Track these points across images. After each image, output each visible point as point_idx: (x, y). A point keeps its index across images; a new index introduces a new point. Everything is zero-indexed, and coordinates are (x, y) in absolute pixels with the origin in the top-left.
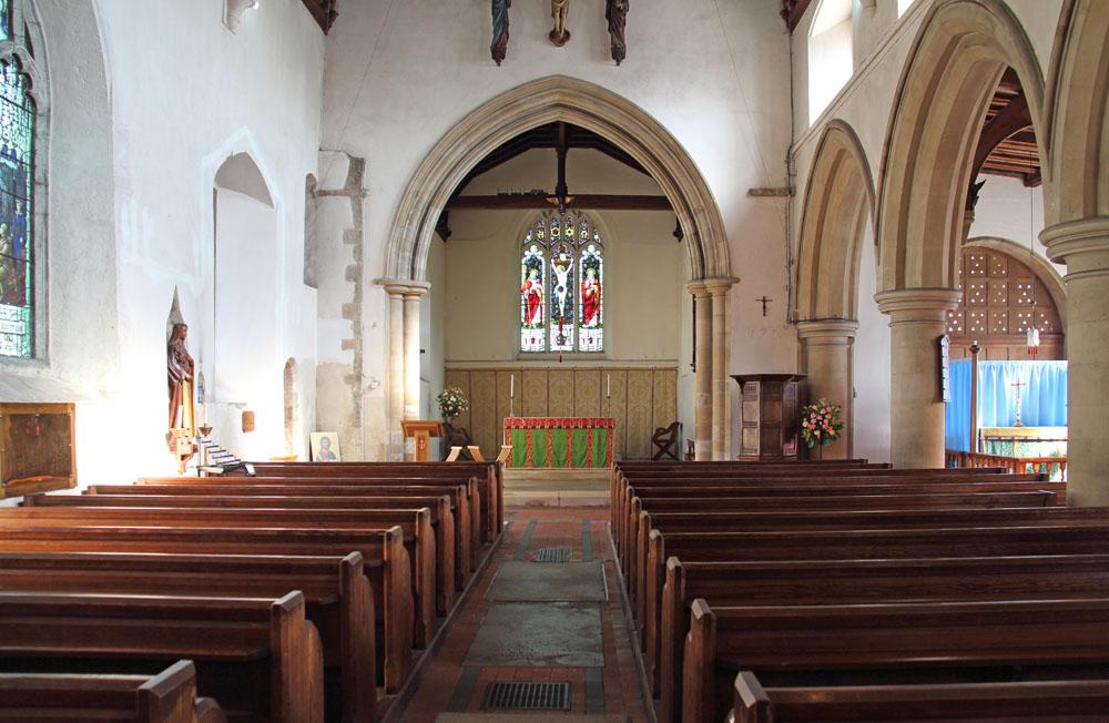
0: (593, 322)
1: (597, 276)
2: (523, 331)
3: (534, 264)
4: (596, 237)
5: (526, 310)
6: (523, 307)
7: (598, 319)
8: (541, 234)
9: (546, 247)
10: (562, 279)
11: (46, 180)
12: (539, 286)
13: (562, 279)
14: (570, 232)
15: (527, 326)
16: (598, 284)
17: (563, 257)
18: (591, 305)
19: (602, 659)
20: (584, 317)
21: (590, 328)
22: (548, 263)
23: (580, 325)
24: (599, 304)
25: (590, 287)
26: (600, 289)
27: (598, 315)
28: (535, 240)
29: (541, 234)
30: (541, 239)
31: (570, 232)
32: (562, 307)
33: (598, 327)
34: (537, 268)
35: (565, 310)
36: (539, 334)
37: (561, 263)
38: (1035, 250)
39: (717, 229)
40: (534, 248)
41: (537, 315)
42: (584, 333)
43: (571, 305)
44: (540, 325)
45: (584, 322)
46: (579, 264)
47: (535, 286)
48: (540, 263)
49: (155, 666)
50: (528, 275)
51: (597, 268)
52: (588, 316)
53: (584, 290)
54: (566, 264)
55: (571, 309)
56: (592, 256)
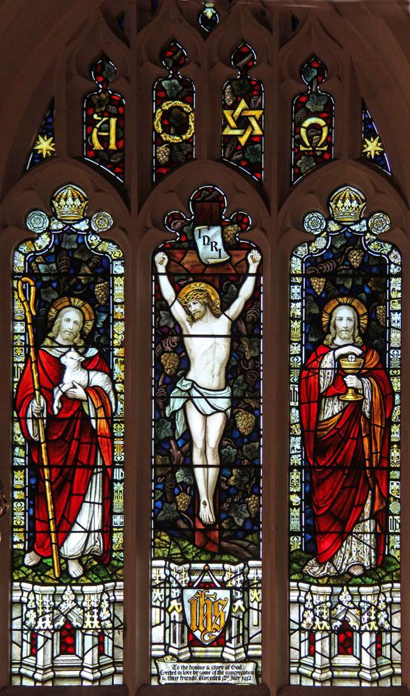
0: (356, 551)
1: (372, 336)
2: (22, 591)
3: (71, 273)
4: (372, 147)
5: (35, 494)
6: (19, 479)
7: (381, 536)
8: (106, 133)
9: (125, 184)
10: (208, 353)
11: (20, 409)
12: (99, 379)
13: (208, 353)
14: (244, 122)
15: (40, 568)
16: (379, 374)
17: (210, 244)
18: (344, 473)
19: (308, 103)
20: (310, 530)
21: (342, 579)
22: (141, 274)
23: (287, 568)
24: (384, 468)
25: (339, 386)
26: (387, 394)
27: (381, 517)
28: (74, 152)
29: (106, 133)
30: (105, 155)
31: (244, 122)
32: (205, 479)
33: (378, 572)
34: (88, 297)
35: (220, 495)
36: (93, 603)
37: (204, 273)
38: (72, 535)
39: (236, 554)
40: (69, 202)
41: (89, 516)
42: (309, 601)
43: (251, 470)
44: (99, 565)
45: (313, 551)
46: (287, 278)
47: (75, 378)
48: (102, 269)
49: (235, 564)
50: (43, 326)
51: (375, 300)
52: (328, 528)
53: (312, 400)
54: (224, 280)
55: (250, 485)
56: (354, 240)
